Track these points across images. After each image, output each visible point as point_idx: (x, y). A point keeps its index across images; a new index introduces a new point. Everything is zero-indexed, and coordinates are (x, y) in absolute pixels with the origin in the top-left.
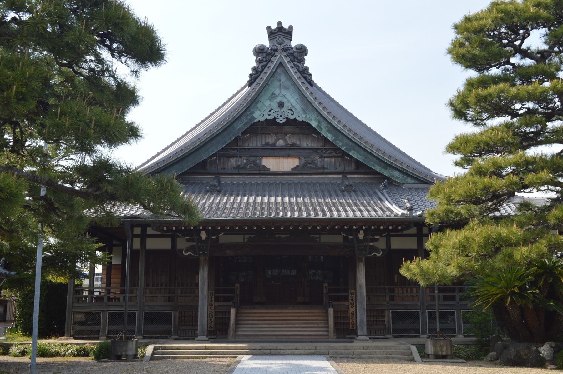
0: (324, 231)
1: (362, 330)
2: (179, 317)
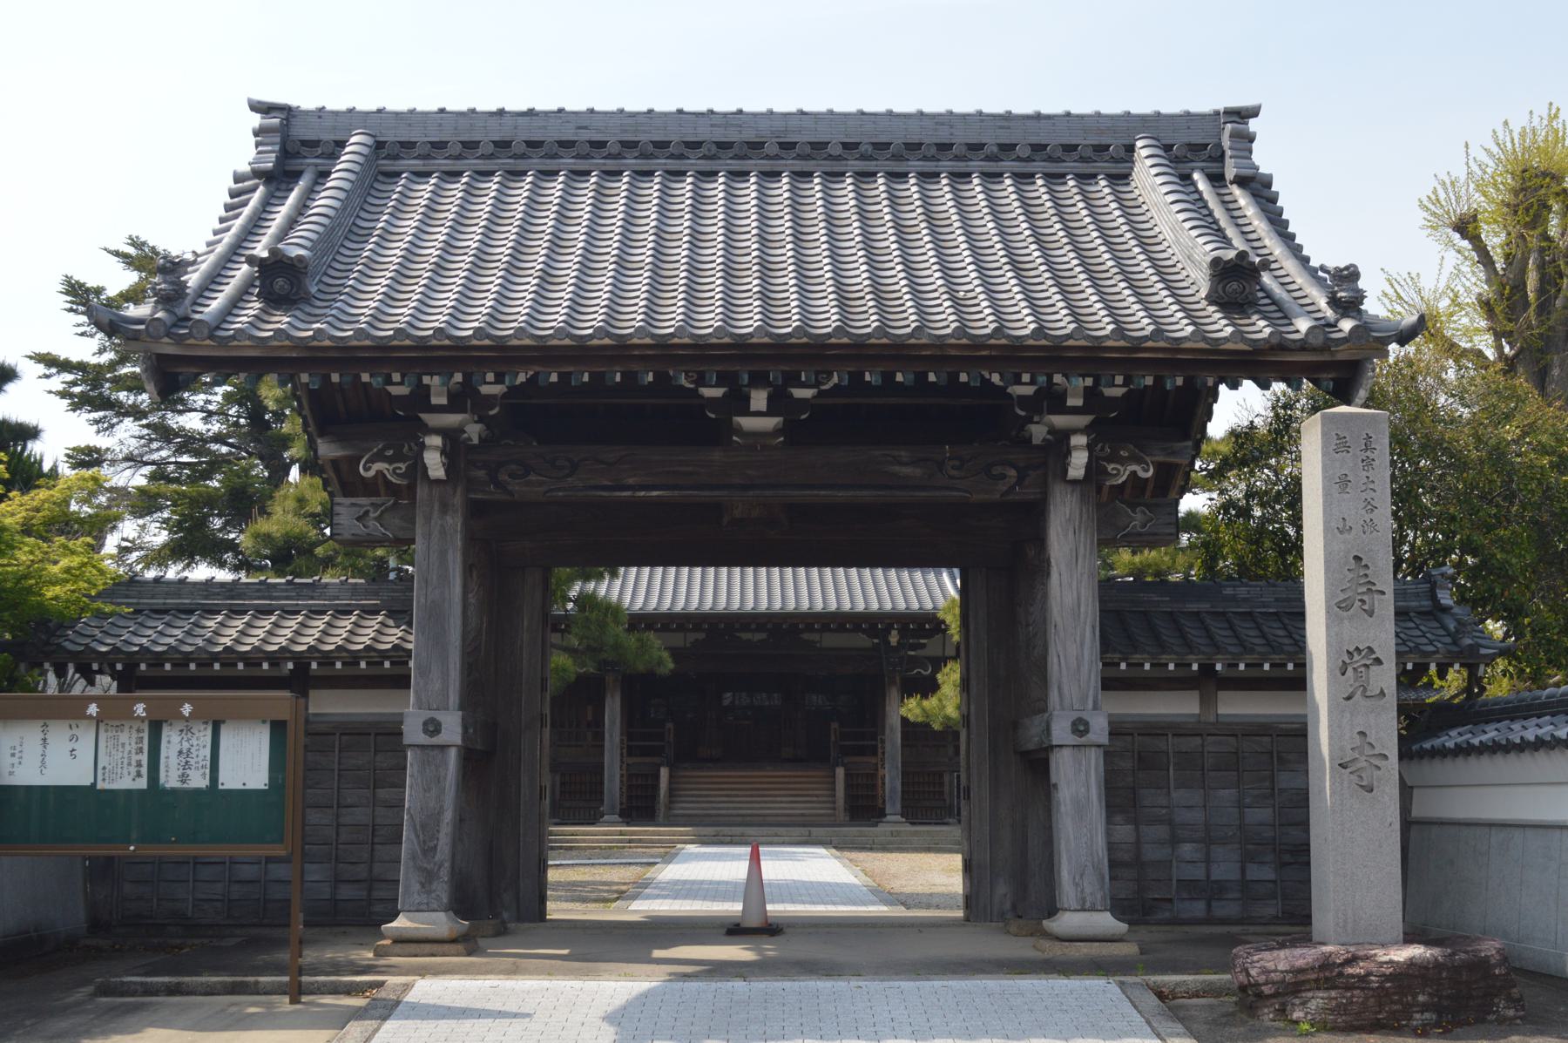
0: (825, 628)
1: (893, 807)
2: (563, 784)
